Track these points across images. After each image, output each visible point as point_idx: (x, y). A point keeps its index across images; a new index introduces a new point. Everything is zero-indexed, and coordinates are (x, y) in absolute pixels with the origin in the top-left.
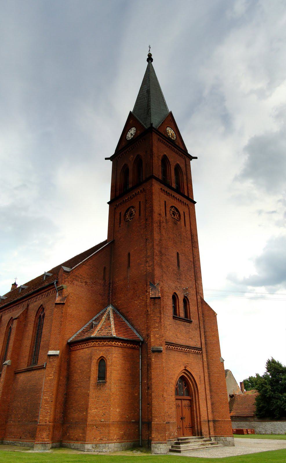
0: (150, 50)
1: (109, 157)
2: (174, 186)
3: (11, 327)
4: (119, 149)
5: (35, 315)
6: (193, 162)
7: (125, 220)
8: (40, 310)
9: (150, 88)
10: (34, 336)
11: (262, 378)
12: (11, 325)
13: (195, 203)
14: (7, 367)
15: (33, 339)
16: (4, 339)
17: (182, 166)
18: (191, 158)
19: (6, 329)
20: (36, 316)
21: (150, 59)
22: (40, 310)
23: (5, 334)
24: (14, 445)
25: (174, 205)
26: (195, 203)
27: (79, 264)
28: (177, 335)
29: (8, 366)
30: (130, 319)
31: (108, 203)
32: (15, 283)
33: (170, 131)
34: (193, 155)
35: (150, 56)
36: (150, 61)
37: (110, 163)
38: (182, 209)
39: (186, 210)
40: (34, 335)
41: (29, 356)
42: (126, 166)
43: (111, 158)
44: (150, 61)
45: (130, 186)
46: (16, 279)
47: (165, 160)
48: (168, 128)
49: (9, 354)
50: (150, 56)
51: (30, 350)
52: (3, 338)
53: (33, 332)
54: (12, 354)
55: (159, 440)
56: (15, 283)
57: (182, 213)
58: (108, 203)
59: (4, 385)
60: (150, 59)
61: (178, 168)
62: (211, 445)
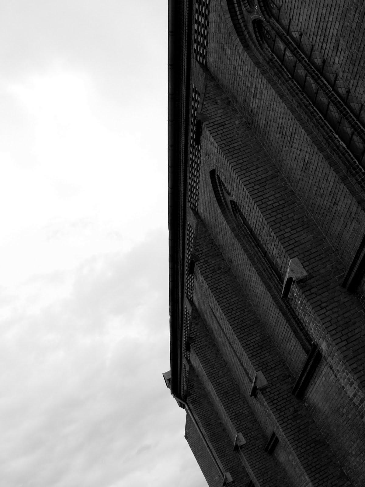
3: (232, 202)
5: (241, 48)
8: (241, 10)
10: (295, 106)
12: (228, 199)
14: (302, 288)
15: (303, 115)
16: (246, 251)
19: (228, 222)
20: (246, 47)
22: (241, 10)
23: (236, 236)
29: (302, 282)
30: (300, 35)
41: (344, 179)
49: (274, 249)
51: (327, 158)
52: (242, 252)
53: (282, 96)
54: (281, 239)
59: (345, 357)
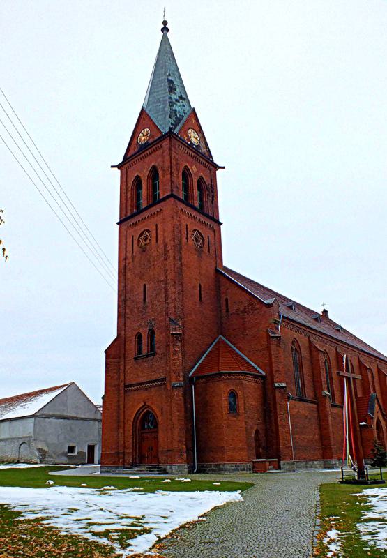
0: (164, 16)
1: (116, 164)
2: (197, 204)
4: (129, 156)
6: (219, 173)
7: (138, 245)
9: (167, 78)
11: (321, 395)
13: (221, 224)
17: (207, 180)
18: (216, 167)
21: (165, 29)
24: (19, 438)
25: (194, 228)
26: (221, 224)
27: (248, 360)
28: (138, 375)
31: (118, 223)
32: (324, 310)
33: (194, 137)
34: (219, 165)
35: (165, 23)
36: (165, 31)
37: (117, 172)
38: (206, 233)
39: (211, 234)
40: (272, 414)
42: (138, 179)
43: (119, 167)
44: (165, 31)
45: (145, 206)
46: (323, 305)
47: (186, 175)
48: (190, 130)
50: (165, 23)
55: (293, 408)
56: (324, 310)
57: (206, 239)
58: (118, 223)
60: (165, 29)
61: (201, 181)
62: (93, 535)
